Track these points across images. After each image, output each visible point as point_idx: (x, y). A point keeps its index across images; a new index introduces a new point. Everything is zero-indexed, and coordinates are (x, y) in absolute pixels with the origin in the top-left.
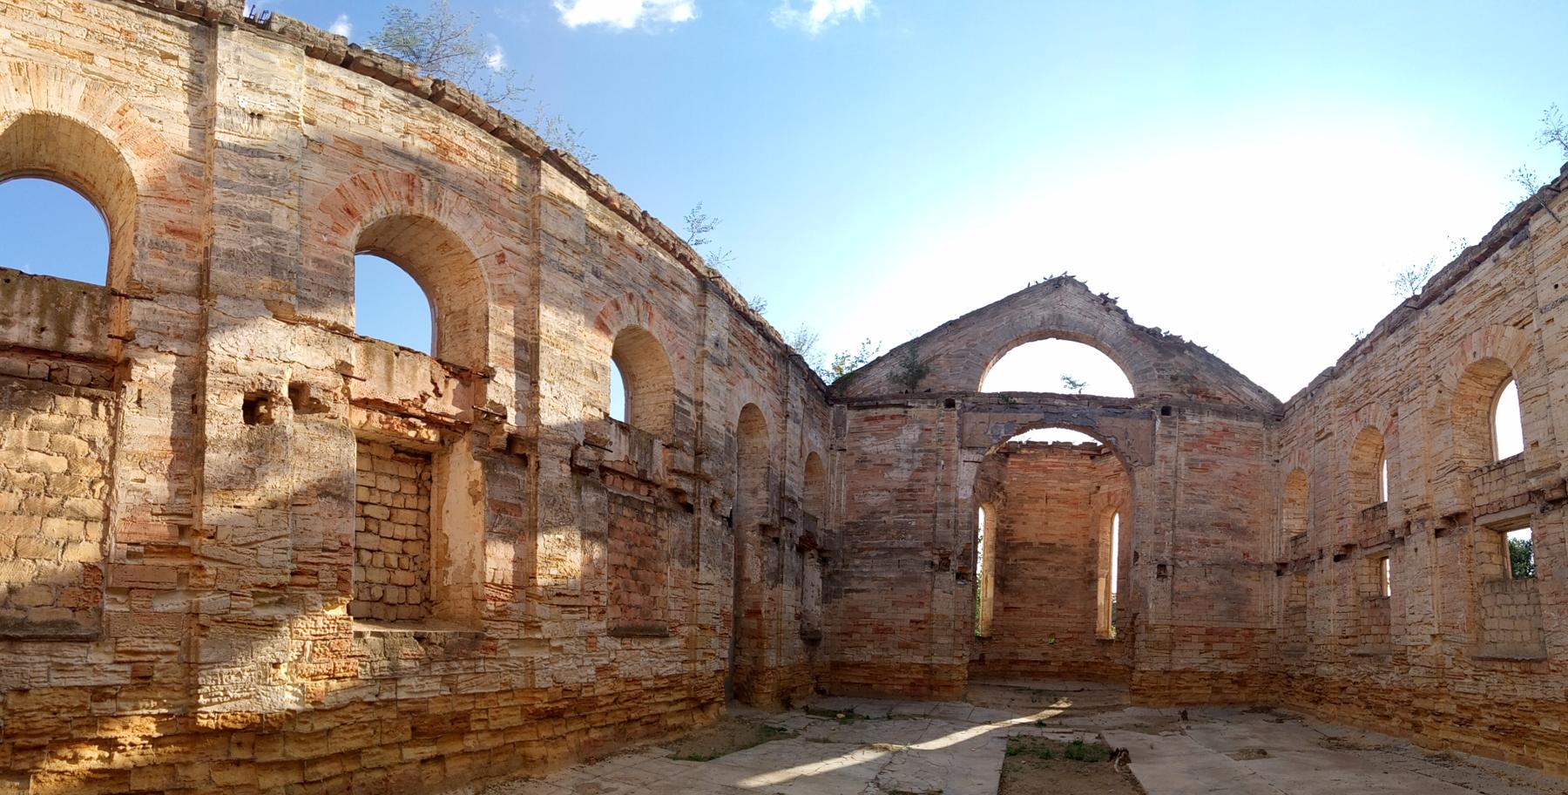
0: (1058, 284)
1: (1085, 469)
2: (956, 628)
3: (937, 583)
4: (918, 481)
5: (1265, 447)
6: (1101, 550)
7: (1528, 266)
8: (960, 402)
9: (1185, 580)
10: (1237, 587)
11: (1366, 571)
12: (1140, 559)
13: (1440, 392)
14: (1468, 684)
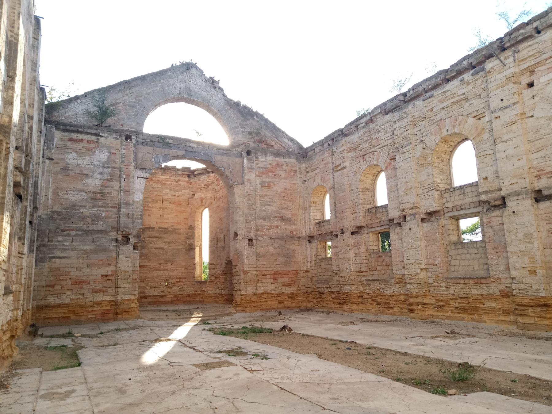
0: (188, 67)
1: (184, 184)
2: (133, 278)
3: (121, 252)
4: (108, 187)
5: (298, 173)
6: (197, 231)
7: (483, 86)
8: (135, 137)
9: (262, 247)
10: (288, 249)
11: (371, 239)
12: (238, 236)
13: (424, 149)
14: (443, 290)
